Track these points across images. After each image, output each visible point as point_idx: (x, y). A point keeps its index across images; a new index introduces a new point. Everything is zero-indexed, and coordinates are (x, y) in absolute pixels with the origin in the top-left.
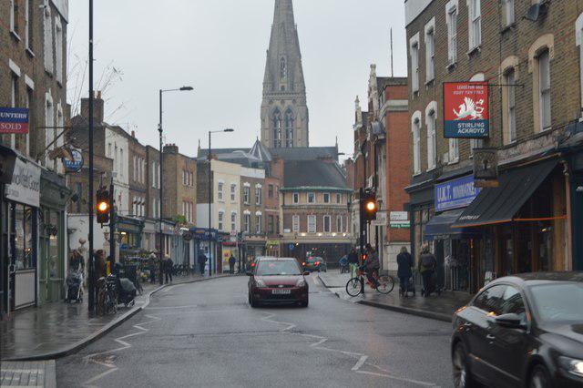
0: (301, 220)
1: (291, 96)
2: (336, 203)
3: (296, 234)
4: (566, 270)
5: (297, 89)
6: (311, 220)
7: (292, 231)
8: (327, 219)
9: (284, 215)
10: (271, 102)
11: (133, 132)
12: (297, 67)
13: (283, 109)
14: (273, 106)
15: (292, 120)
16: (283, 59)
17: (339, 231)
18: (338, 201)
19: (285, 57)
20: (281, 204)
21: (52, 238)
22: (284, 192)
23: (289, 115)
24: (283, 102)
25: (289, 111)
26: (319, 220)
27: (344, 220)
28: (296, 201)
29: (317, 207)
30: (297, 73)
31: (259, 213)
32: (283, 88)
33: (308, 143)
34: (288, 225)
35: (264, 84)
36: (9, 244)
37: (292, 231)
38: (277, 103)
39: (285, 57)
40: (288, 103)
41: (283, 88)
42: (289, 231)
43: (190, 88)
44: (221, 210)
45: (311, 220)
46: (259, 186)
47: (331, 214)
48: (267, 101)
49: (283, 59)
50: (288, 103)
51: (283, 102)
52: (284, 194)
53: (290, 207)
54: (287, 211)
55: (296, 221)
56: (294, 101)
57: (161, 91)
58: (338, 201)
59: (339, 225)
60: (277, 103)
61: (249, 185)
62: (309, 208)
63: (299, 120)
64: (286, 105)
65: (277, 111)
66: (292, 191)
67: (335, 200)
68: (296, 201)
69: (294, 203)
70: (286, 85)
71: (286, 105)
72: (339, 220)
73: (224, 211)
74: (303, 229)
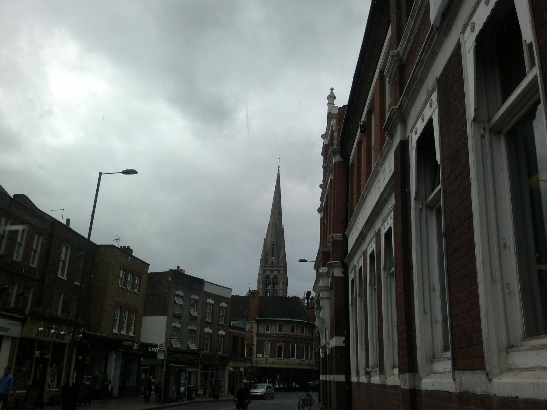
1: (277, 268)
2: (301, 334)
3: (267, 359)
4: (206, 319)
5: (281, 264)
7: (263, 356)
8: (293, 346)
9: (258, 341)
10: (264, 272)
11: (68, 221)
12: (282, 249)
13: (272, 276)
14: (266, 274)
15: (277, 284)
17: (303, 358)
18: (302, 332)
19: (275, 244)
20: (255, 332)
22: (258, 322)
23: (275, 280)
24: (272, 272)
25: (275, 277)
26: (273, 347)
27: (307, 349)
28: (268, 330)
29: (284, 336)
30: (282, 254)
31: (222, 332)
32: (272, 263)
33: (287, 293)
34: (260, 350)
37: (263, 356)
38: (268, 272)
39: (275, 244)
40: (275, 272)
41: (272, 263)
42: (261, 356)
43: (133, 172)
46: (224, 304)
47: (296, 343)
48: (262, 271)
49: (273, 245)
50: (275, 272)
51: (272, 272)
53: (263, 335)
54: (260, 338)
56: (279, 272)
57: (101, 174)
58: (302, 332)
59: (303, 352)
60: (268, 272)
61: (213, 302)
62: (278, 336)
63: (281, 284)
64: (274, 274)
65: (268, 277)
66: (265, 321)
67: (300, 331)
68: (268, 330)
69: (266, 332)
70: (274, 261)
71: (274, 274)
72: (303, 348)
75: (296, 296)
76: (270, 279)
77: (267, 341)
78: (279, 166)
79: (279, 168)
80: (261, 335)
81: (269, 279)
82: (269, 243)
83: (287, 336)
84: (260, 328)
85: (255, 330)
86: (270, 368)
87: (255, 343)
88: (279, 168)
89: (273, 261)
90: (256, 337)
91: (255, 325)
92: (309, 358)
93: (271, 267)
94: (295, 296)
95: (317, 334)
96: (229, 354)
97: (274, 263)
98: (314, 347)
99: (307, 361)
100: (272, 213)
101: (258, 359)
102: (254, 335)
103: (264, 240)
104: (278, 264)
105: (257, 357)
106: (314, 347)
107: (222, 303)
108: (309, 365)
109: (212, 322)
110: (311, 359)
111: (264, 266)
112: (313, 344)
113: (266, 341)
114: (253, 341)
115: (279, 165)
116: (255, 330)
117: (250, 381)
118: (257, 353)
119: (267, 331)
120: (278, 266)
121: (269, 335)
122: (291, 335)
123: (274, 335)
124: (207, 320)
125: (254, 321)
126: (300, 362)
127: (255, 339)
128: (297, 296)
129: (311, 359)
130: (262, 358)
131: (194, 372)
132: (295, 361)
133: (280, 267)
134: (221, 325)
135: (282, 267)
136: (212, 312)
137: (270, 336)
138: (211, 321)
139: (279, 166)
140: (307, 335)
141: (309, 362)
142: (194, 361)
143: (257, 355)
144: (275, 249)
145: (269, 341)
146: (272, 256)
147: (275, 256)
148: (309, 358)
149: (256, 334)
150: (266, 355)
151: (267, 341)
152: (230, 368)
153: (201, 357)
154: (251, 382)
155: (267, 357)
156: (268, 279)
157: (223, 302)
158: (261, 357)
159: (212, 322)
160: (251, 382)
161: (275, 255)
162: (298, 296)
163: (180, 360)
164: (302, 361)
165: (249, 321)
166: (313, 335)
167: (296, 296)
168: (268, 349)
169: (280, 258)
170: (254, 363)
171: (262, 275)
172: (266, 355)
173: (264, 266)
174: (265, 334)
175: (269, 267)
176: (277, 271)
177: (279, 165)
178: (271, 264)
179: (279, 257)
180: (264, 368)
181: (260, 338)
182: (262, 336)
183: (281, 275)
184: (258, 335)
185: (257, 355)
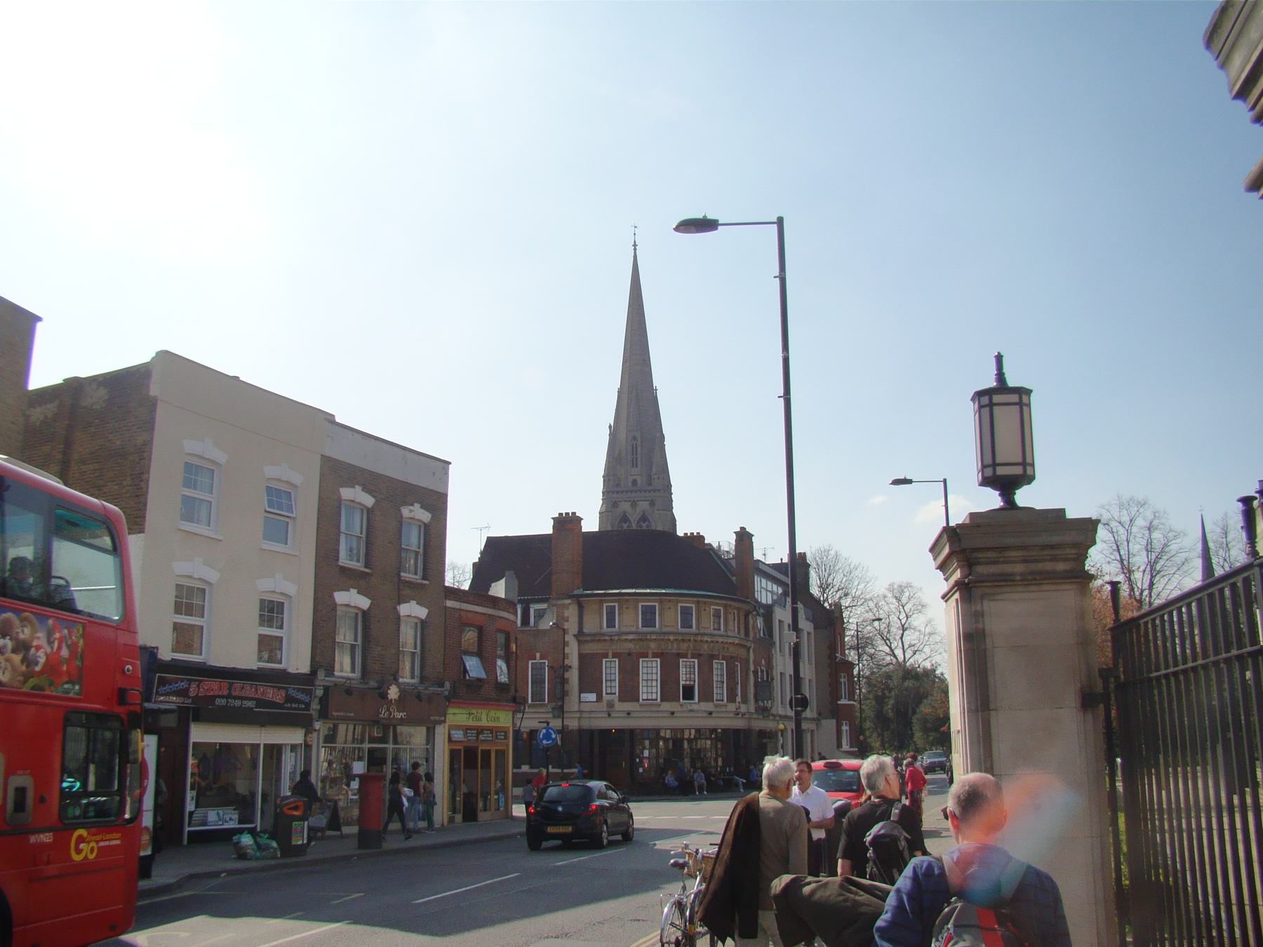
0: (622, 670)
1: (647, 494)
3: (611, 705)
6: (650, 673)
7: (600, 698)
16: (634, 438)
19: (638, 435)
21: (709, 742)
24: (634, 504)
28: (611, 623)
34: (590, 681)
35: (604, 477)
36: (17, 698)
37: (600, 698)
38: (625, 506)
39: (638, 435)
42: (592, 697)
44: (194, 568)
45: (650, 673)
49: (634, 438)
51: (634, 504)
52: (581, 607)
53: (597, 637)
55: (611, 670)
56: (652, 503)
60: (625, 506)
64: (639, 509)
68: (611, 623)
73: (212, 575)
74: (629, 691)
75: (695, 534)
76: (630, 521)
77: (610, 655)
78: (635, 245)
79: (635, 249)
80: (589, 638)
81: (628, 523)
82: (623, 435)
83: (672, 638)
84: (586, 618)
85: (572, 626)
86: (620, 731)
87: (574, 660)
88: (635, 249)
89: (635, 477)
90: (577, 644)
91: (572, 612)
92: (739, 699)
93: (631, 492)
94: (692, 534)
95: (760, 633)
96: (448, 685)
97: (639, 482)
98: (752, 668)
99: (732, 707)
100: (626, 362)
101: (585, 707)
102: (569, 638)
103: (610, 427)
104: (650, 484)
105: (580, 702)
106: (752, 668)
107: (411, 508)
108: (740, 716)
109: (367, 570)
110: (745, 700)
111: (613, 492)
112: (747, 661)
113: (606, 656)
114: (564, 656)
115: (635, 242)
116: (572, 626)
117: (559, 771)
118: (582, 690)
119: (608, 627)
120: (650, 488)
121: (616, 638)
122: (682, 634)
123: (631, 637)
124: (344, 560)
125: (568, 601)
126: (710, 710)
127: (573, 651)
128: (698, 533)
129: (745, 700)
130: (596, 704)
131: (294, 748)
132: (695, 707)
133: (654, 491)
134: (410, 584)
135: (659, 490)
136: (367, 537)
137: (619, 640)
138: (366, 567)
139: (635, 245)
140: (730, 634)
141: (739, 708)
142: (287, 708)
143: (580, 696)
144: (639, 449)
145: (615, 655)
146: (633, 467)
147: (639, 466)
148: (739, 699)
149: (574, 635)
150: (607, 694)
151: (610, 655)
152: (452, 732)
153: (320, 692)
154: (565, 771)
155: (613, 701)
156: (625, 523)
157: (412, 505)
158: (595, 700)
159: (367, 570)
160: (565, 771)
161: (639, 463)
162: (701, 534)
163: (219, 702)
164: (716, 706)
165: (555, 602)
166: (747, 634)
167: (695, 534)
168: (613, 678)
169: (654, 470)
170: (586, 718)
171: (610, 514)
172: (607, 694)
173: (613, 492)
174: (604, 635)
175: (627, 492)
176: (647, 503)
177: (635, 242)
178: (630, 484)
179: (651, 468)
180: (605, 733)
181: (591, 648)
182: (592, 641)
183: (658, 510)
184: (580, 635)
185: (582, 695)
